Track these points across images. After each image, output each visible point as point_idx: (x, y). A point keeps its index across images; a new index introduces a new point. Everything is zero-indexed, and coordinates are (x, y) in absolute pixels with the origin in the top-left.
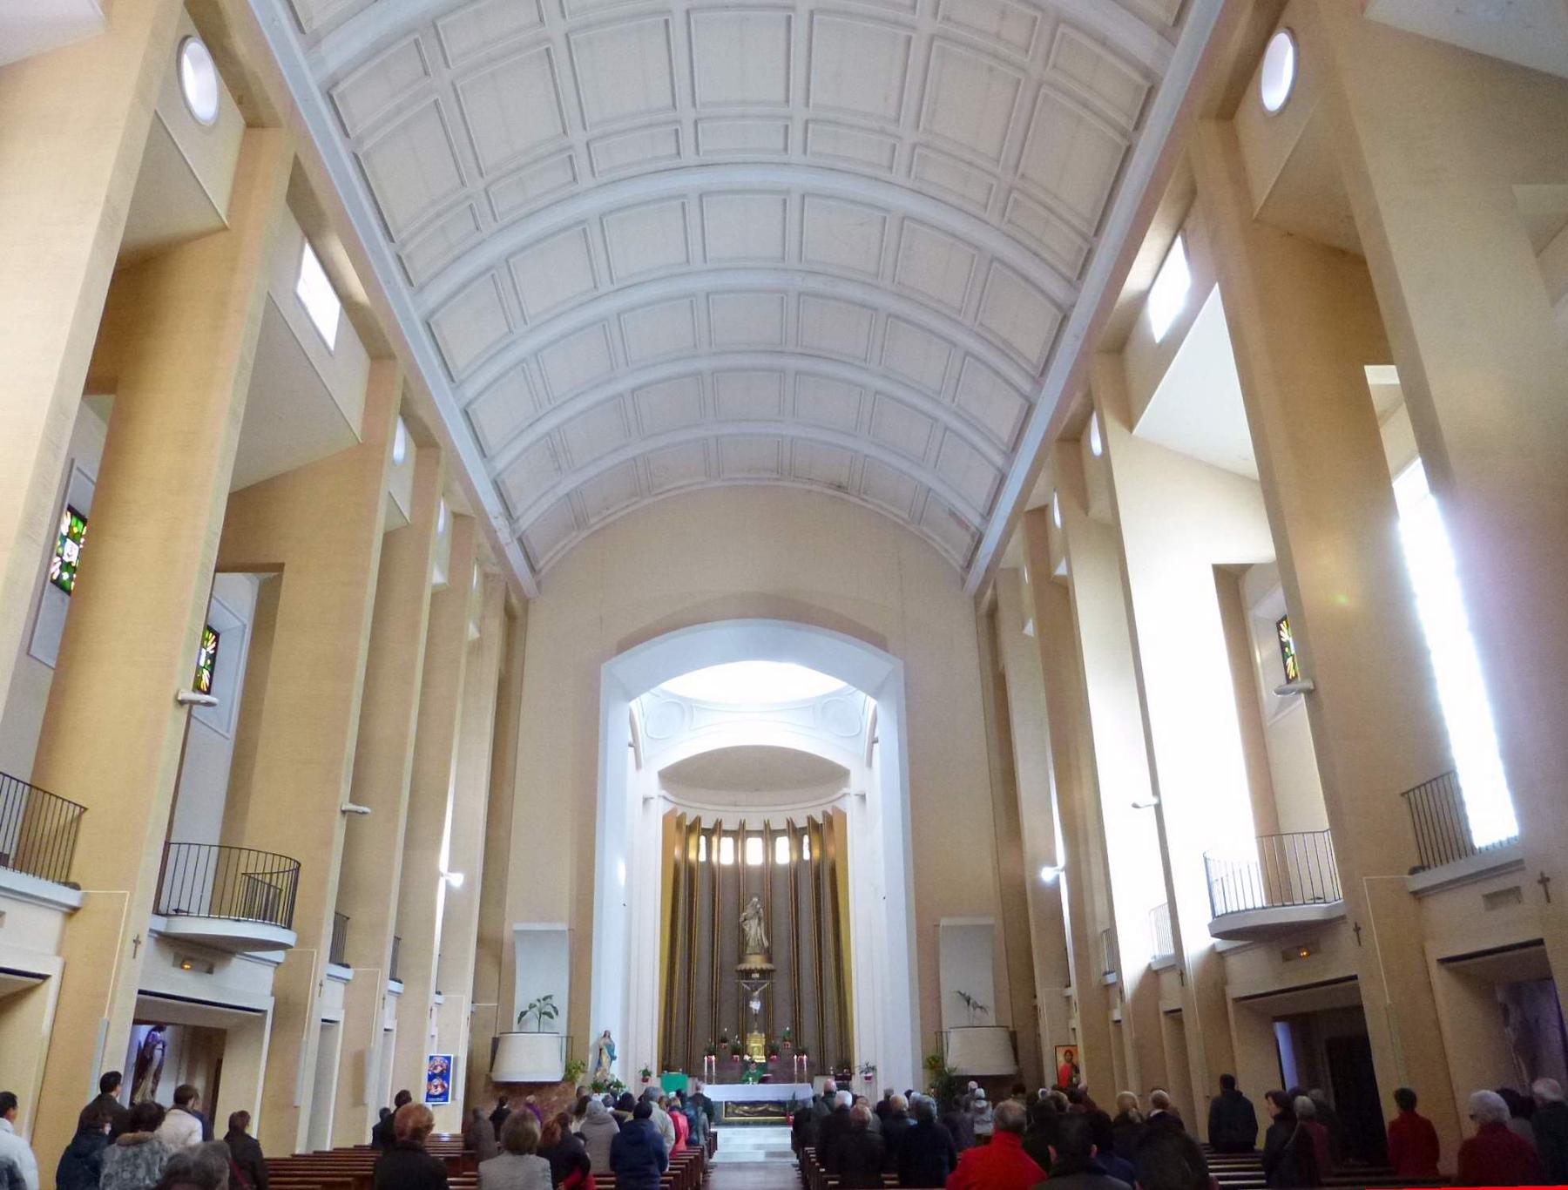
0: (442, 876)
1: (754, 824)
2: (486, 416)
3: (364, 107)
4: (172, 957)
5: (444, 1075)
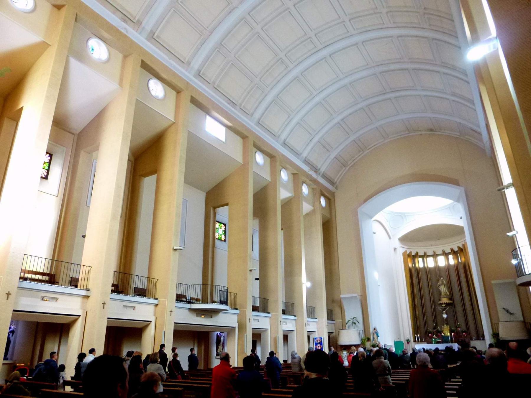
0: (303, 284)
1: (430, 253)
2: (291, 142)
3: (211, 74)
4: (196, 315)
5: (321, 343)
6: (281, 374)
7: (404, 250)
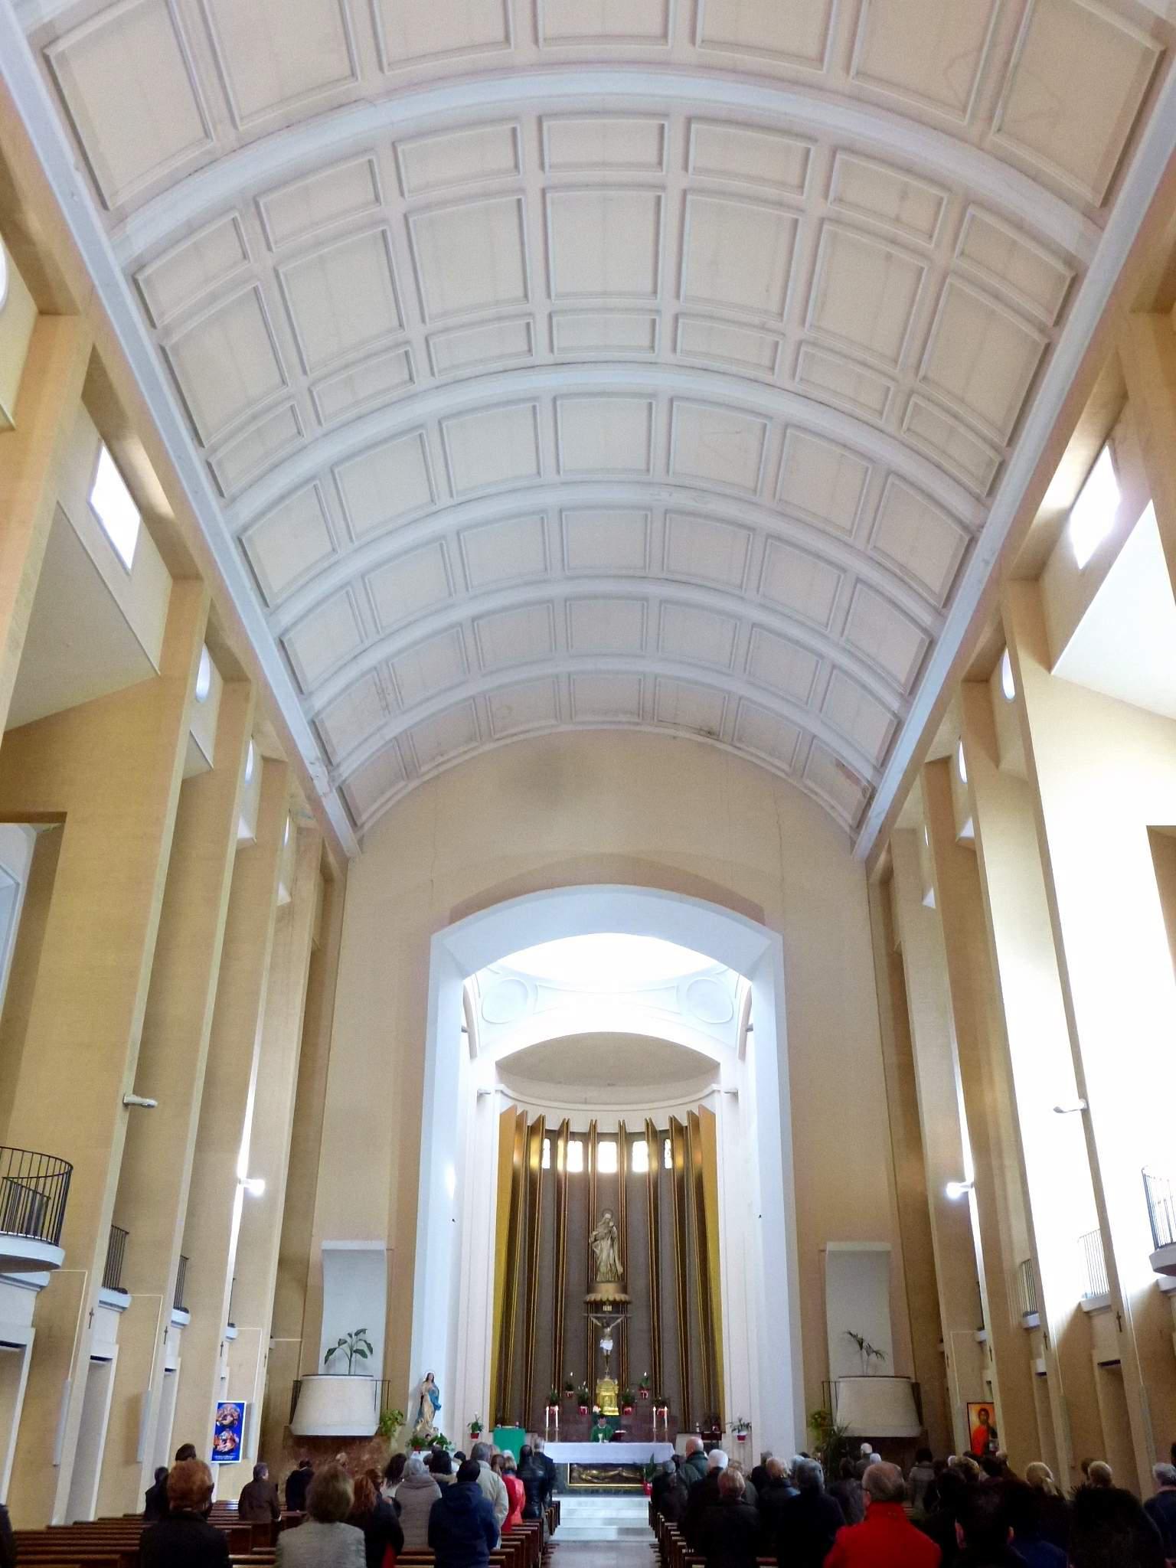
1: (579, 1126)
6: (399, 1557)
7: (508, 1104)
